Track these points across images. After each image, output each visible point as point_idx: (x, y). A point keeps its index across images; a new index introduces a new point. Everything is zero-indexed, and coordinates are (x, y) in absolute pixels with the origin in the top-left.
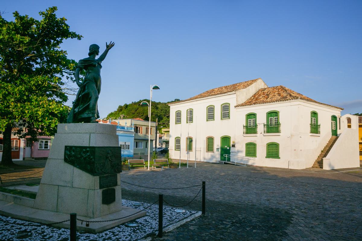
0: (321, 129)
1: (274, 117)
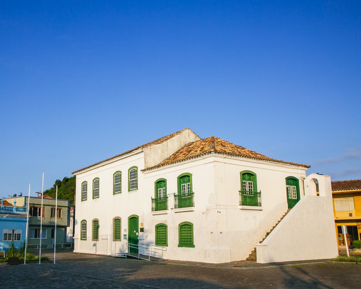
0: (263, 199)
1: (187, 184)
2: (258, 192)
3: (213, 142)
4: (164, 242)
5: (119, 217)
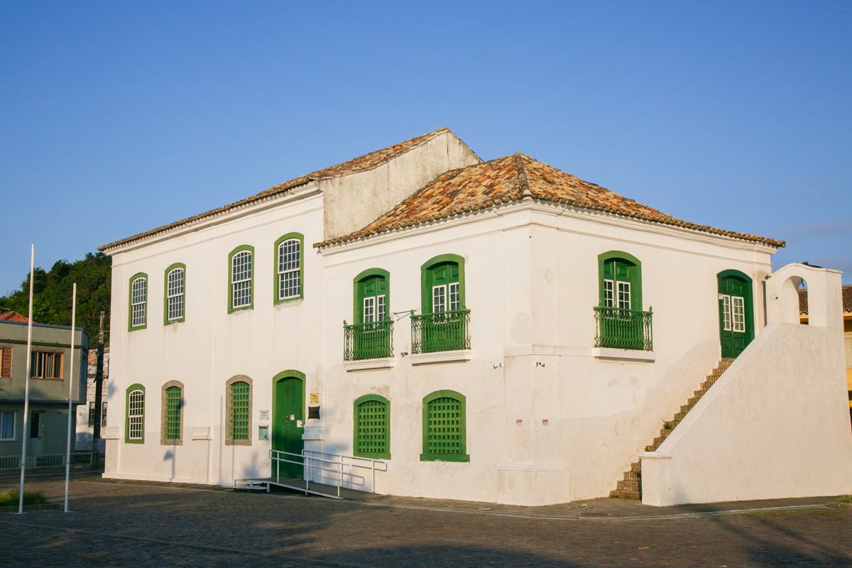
0: (659, 331)
1: (450, 285)
2: (644, 310)
3: (520, 171)
4: (381, 447)
5: (244, 376)
